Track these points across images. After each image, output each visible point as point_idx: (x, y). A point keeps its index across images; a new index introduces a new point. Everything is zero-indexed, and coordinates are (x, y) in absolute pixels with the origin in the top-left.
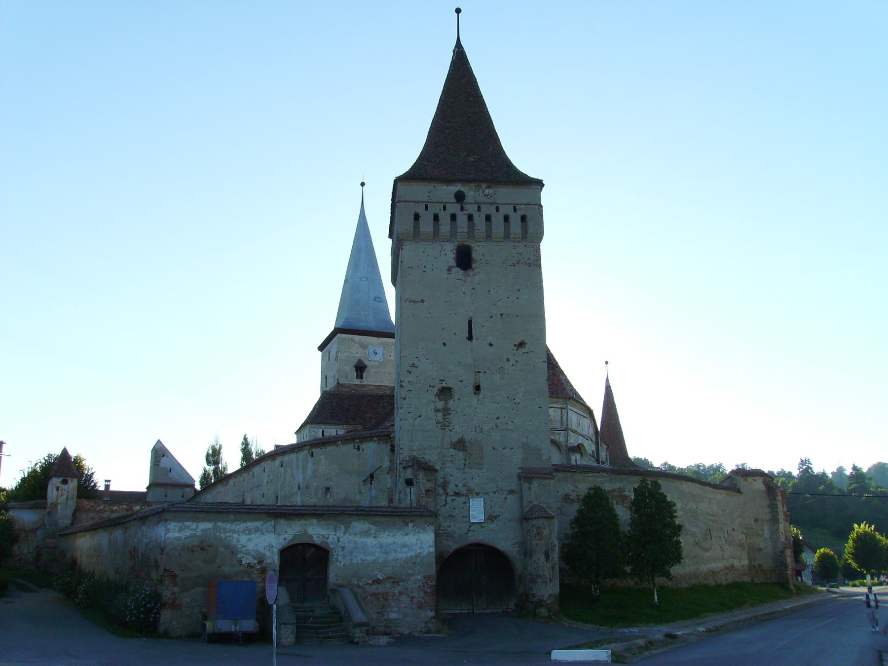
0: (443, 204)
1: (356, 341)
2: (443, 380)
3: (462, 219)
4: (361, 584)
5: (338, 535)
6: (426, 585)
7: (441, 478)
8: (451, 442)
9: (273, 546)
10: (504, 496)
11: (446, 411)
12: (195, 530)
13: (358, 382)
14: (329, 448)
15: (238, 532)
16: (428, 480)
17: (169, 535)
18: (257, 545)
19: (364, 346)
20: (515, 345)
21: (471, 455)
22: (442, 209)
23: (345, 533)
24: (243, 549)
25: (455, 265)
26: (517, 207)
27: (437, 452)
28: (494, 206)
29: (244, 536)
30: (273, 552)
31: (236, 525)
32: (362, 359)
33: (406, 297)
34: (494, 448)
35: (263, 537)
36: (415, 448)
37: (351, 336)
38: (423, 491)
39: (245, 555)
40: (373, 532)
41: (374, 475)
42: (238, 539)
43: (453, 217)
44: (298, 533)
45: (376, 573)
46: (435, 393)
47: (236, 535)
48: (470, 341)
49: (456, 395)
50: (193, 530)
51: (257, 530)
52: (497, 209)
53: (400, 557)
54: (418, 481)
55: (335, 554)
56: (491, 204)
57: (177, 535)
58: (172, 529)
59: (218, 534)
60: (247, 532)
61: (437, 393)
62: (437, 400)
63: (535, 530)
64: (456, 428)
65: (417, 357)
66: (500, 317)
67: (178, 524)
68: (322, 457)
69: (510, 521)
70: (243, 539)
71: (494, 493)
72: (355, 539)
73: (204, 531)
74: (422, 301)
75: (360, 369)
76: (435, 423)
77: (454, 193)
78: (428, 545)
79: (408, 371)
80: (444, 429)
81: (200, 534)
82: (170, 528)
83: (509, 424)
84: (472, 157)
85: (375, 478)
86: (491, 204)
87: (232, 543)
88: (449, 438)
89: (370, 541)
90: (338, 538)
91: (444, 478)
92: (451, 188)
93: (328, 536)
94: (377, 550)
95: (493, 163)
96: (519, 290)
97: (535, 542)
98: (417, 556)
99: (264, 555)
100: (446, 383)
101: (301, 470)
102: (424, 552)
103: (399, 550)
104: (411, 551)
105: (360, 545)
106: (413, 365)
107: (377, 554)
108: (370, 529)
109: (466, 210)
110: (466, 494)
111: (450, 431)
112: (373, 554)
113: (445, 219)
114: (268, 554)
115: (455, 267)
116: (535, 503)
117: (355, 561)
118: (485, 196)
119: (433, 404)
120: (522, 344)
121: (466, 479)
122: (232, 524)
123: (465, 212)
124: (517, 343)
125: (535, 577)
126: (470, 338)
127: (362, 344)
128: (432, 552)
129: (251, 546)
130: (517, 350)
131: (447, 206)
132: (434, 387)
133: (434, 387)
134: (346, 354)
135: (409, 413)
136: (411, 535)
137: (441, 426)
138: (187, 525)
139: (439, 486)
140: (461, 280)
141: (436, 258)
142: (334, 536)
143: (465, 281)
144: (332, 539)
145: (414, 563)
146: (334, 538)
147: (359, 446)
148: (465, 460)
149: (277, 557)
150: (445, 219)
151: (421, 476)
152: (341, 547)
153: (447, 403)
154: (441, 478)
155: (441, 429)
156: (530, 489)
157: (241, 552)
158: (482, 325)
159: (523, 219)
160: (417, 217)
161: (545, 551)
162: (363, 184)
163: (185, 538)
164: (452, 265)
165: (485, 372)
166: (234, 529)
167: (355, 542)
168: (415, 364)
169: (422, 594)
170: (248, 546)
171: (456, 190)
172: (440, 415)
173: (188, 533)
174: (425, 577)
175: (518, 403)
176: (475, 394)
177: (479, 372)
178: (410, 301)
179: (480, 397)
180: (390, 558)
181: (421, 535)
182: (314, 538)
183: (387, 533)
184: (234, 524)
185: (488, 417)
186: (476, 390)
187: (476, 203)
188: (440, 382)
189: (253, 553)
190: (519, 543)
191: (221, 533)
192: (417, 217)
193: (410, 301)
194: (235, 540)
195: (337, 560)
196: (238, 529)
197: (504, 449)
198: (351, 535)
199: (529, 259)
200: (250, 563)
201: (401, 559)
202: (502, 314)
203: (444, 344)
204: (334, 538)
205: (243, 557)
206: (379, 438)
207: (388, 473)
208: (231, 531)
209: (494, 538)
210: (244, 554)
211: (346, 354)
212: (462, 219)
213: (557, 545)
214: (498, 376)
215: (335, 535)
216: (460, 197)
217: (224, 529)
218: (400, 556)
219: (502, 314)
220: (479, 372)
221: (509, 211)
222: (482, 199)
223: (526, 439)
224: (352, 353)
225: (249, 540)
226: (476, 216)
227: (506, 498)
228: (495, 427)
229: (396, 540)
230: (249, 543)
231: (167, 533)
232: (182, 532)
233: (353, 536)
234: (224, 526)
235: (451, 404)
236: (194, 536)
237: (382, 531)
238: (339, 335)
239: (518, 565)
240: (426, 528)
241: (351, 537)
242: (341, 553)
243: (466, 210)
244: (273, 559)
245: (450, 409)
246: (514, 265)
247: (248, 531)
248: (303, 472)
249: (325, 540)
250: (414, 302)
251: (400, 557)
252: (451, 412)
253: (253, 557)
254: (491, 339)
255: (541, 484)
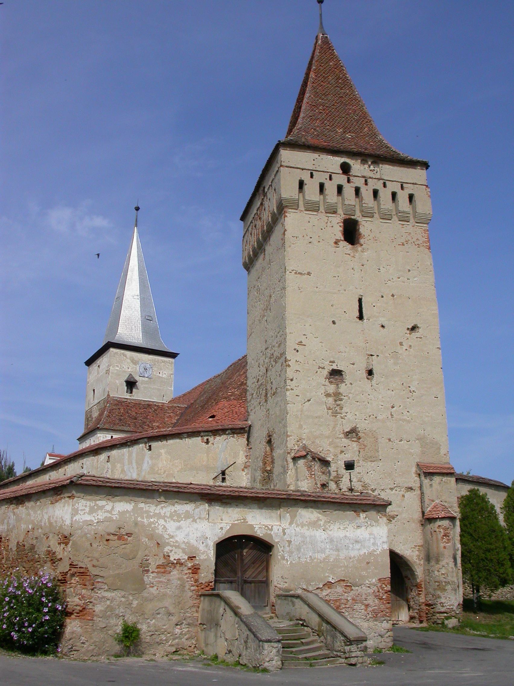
0: (330, 173)
1: (128, 357)
2: (333, 362)
3: (349, 190)
4: (310, 588)
5: (283, 525)
6: (381, 590)
7: (334, 471)
8: (343, 431)
9: (207, 538)
10: (402, 493)
11: (337, 396)
12: (110, 512)
13: (127, 396)
14: (171, 442)
15: (164, 517)
16: (323, 473)
17: (77, 518)
18: (187, 535)
19: (135, 362)
20: (408, 329)
21: (365, 446)
22: (328, 179)
23: (291, 524)
24: (171, 540)
25: (343, 239)
26: (405, 185)
27: (328, 442)
28: (382, 182)
29: (172, 522)
30: (207, 546)
31: (162, 508)
32: (132, 374)
33: (292, 268)
34: (390, 440)
35: (195, 525)
36: (304, 436)
37: (122, 351)
38: (319, 486)
39: (174, 548)
40: (322, 523)
41: (227, 472)
42: (165, 526)
43: (340, 189)
44: (236, 522)
45: (327, 574)
46: (325, 376)
47: (161, 522)
48: (360, 321)
49: (348, 377)
50: (108, 511)
51: (187, 515)
52: (385, 185)
53: (352, 556)
54: (313, 473)
55: (280, 549)
56: (379, 179)
57: (88, 518)
58: (81, 510)
59: (139, 519)
60: (175, 518)
61: (327, 375)
62: (327, 383)
63: (442, 530)
64: (349, 416)
65: (304, 335)
66: (392, 297)
67: (88, 503)
68: (163, 451)
69: (408, 522)
70: (171, 526)
71: (392, 489)
72: (302, 531)
73: (121, 513)
74: (309, 274)
75: (131, 384)
76: (326, 409)
77: (339, 164)
78: (381, 541)
79: (295, 349)
80: (336, 416)
81: (116, 517)
82: (78, 508)
83: (404, 414)
84: (349, 134)
85: (227, 475)
86: (379, 179)
87: (157, 531)
88: (341, 426)
89: (319, 535)
90: (284, 530)
91: (337, 471)
92: (337, 158)
93: (272, 527)
94: (328, 547)
95: (371, 142)
96: (409, 271)
97: (442, 545)
98: (371, 554)
99: (197, 549)
100: (337, 365)
101: (134, 464)
102: (378, 549)
103: (351, 546)
104: (364, 548)
105: (308, 539)
106: (300, 343)
107: (327, 552)
108: (319, 519)
109: (352, 182)
110: (361, 490)
111: (342, 418)
112: (323, 551)
113: (331, 189)
114: (202, 548)
115: (342, 240)
116: (437, 501)
117: (303, 560)
118: (371, 171)
119: (323, 387)
120: (414, 328)
121: (360, 473)
122: (156, 506)
123: (352, 184)
124: (410, 327)
125: (444, 584)
126: (361, 317)
127: (133, 359)
128: (387, 549)
129: (180, 537)
130: (410, 334)
131: (333, 175)
132: (323, 368)
133: (323, 368)
134: (117, 368)
135: (297, 396)
136: (363, 528)
137: (332, 413)
138: (100, 505)
139: (332, 480)
140: (349, 255)
141: (322, 229)
142: (278, 527)
143: (354, 257)
144: (276, 531)
145: (368, 563)
146: (278, 530)
147: (207, 439)
148: (359, 452)
149: (212, 552)
150: (331, 189)
151: (316, 468)
152: (287, 541)
153: (338, 388)
154: (334, 471)
155: (332, 416)
156: (431, 485)
157: (168, 544)
158: (374, 305)
159: (411, 197)
160: (301, 184)
161: (454, 554)
162: (137, 209)
163: (97, 522)
164: (339, 239)
165: (378, 356)
166: (160, 513)
167: (303, 536)
168: (303, 341)
169: (377, 601)
170: (176, 535)
171: (342, 162)
172: (331, 400)
173: (101, 515)
174: (380, 580)
175: (413, 391)
176: (368, 379)
177: (372, 355)
178: (296, 273)
179: (374, 382)
180: (342, 556)
181: (374, 528)
182: (256, 529)
183: (337, 525)
184: (159, 507)
185: (382, 405)
186: (368, 375)
187: (363, 177)
188: (330, 364)
189: (183, 546)
190: (418, 546)
191: (143, 518)
192: (301, 184)
193: (296, 273)
194: (160, 528)
195: (283, 558)
196: (165, 513)
197: (400, 441)
198: (298, 525)
199: (417, 239)
200: (179, 559)
201: (354, 557)
202: (393, 294)
203: (334, 322)
204: (278, 530)
205: (171, 551)
206: (234, 431)
207: (243, 470)
208: (155, 515)
209: (393, 540)
210: (172, 546)
211: (117, 368)
212: (349, 190)
213: (460, 549)
214: (392, 361)
215: (280, 526)
216: (345, 169)
217: (147, 512)
218: (353, 554)
219: (393, 294)
220: (372, 355)
221: (396, 188)
222: (368, 174)
223: (423, 431)
224: (123, 367)
225: (179, 528)
226: (363, 190)
227: (403, 496)
228: (390, 417)
229: (348, 535)
230: (178, 533)
231: (75, 515)
232: (94, 514)
233: (300, 527)
234: (147, 508)
235: (343, 388)
236: (107, 520)
237: (331, 522)
238: (112, 349)
239: (419, 572)
240: (379, 520)
241: (297, 529)
242: (288, 549)
243: (352, 182)
244: (207, 555)
245: (342, 395)
246: (403, 245)
247: (176, 517)
248: (137, 468)
249: (269, 532)
250: (300, 274)
251: (352, 556)
252: (343, 397)
253: (184, 551)
254: (383, 321)
255: (442, 481)
